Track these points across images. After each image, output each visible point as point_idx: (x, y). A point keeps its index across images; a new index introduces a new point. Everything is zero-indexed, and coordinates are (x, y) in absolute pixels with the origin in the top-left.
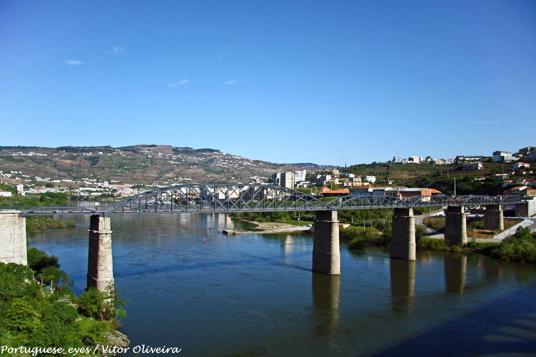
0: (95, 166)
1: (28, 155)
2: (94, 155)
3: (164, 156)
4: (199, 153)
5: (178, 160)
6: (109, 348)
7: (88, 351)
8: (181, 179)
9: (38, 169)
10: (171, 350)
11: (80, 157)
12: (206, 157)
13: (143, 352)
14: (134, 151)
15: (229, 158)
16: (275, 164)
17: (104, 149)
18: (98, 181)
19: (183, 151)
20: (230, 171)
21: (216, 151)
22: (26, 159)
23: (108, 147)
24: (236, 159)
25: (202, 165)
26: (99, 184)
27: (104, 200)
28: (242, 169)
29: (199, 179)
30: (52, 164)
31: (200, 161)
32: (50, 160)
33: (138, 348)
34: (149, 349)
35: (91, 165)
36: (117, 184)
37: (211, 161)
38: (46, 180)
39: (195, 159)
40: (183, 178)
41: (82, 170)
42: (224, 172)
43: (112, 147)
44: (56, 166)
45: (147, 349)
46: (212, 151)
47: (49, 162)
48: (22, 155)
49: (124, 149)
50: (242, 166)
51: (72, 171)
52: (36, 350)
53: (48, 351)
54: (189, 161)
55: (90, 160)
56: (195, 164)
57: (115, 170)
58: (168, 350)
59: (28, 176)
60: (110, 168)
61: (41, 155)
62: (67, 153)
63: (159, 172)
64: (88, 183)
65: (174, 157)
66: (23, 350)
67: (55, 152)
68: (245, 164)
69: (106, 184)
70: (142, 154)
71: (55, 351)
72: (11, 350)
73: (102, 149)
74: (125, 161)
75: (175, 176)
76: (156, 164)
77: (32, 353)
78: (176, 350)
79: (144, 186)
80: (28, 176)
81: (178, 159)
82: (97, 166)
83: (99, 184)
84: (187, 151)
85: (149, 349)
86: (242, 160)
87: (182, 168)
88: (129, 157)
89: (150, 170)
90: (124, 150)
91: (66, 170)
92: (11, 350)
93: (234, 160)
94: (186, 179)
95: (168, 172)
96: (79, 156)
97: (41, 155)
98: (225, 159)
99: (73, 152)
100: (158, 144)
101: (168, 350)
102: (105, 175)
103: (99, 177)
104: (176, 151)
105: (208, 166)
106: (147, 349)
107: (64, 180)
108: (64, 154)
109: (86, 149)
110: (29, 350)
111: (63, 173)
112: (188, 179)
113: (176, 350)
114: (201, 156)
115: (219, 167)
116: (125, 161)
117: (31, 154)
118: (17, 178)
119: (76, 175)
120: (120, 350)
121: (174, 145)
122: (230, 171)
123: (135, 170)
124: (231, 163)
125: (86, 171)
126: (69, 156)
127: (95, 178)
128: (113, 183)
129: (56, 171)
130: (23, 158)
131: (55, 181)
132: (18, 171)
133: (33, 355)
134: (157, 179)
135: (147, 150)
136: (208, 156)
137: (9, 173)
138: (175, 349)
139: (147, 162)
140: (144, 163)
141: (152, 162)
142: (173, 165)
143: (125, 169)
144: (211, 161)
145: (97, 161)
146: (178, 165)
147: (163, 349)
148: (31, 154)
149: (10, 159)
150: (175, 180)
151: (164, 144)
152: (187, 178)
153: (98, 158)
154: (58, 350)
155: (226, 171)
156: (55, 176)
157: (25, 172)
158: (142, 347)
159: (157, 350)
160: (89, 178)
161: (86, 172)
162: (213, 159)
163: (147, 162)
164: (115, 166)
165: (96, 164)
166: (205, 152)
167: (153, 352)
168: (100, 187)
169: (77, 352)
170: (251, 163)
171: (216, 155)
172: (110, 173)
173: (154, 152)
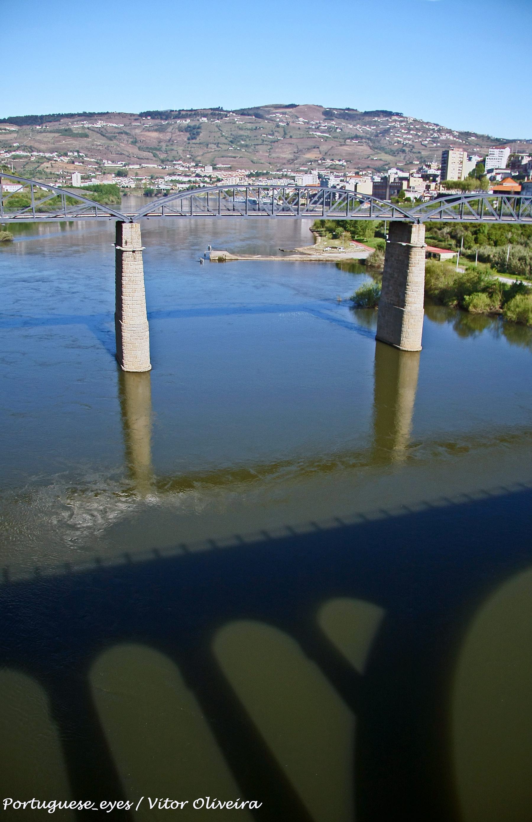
0: (194, 141)
1: (95, 126)
2: (192, 124)
3: (308, 123)
4: (367, 119)
5: (329, 130)
6: (158, 801)
7: (129, 806)
8: (329, 162)
9: (107, 148)
10: (248, 804)
11: (171, 127)
12: (377, 126)
13: (207, 808)
14: (257, 116)
15: (420, 127)
16: (497, 140)
17: (210, 112)
18: (197, 166)
19: (340, 115)
20: (414, 150)
21: (397, 114)
22: (91, 132)
23: (217, 109)
24: (429, 130)
25: (368, 139)
26: (198, 171)
27: (179, 474)
28: (436, 147)
29: (357, 163)
30: (131, 140)
31: (367, 132)
32: (127, 134)
33: (200, 801)
34: (216, 803)
35: (189, 139)
36: (226, 169)
37: (386, 132)
38: (119, 165)
39: (359, 129)
40: (332, 160)
41: (174, 147)
42: (404, 151)
43: (224, 109)
44: (136, 142)
45: (213, 803)
46: (389, 114)
47: (124, 136)
48: (86, 126)
49: (243, 113)
50: (438, 142)
51: (159, 150)
52: (54, 805)
53: (70, 806)
54: (348, 131)
55: (186, 131)
56: (356, 137)
57: (224, 147)
58: (243, 805)
59: (92, 160)
60: (217, 144)
61: (115, 125)
62: (153, 121)
63: (296, 150)
64: (181, 169)
65: (324, 125)
66: (35, 804)
67: (136, 120)
68: (443, 138)
69: (209, 170)
70: (271, 120)
71: (82, 806)
72: (17, 805)
73: (206, 112)
74: (241, 133)
75: (321, 156)
76: (291, 137)
77: (48, 809)
78: (255, 805)
79: (267, 173)
80: (92, 160)
81: (329, 128)
82: (197, 141)
83: (198, 171)
84: (348, 115)
85: (216, 803)
86: (439, 131)
87: (333, 144)
88: (249, 126)
89: (281, 148)
90: (243, 114)
91: (151, 148)
92: (17, 805)
93: (425, 131)
94: (337, 162)
95: (309, 150)
96: (171, 124)
97: (115, 125)
98: (409, 130)
99: (162, 119)
100: (301, 104)
101: (243, 805)
102: (209, 155)
103: (199, 158)
104: (329, 114)
105: (379, 142)
106: (213, 803)
107: (146, 165)
108: (149, 122)
109: (184, 113)
110: (44, 804)
111: (145, 154)
112: (341, 163)
113: (255, 805)
114: (370, 124)
115: (399, 142)
116: (241, 133)
117: (99, 124)
118: (76, 163)
119: (165, 155)
120: (175, 805)
121: (327, 105)
122: (414, 150)
123: (257, 147)
124: (419, 137)
125: (180, 149)
126: (157, 125)
127: (193, 161)
128: (220, 169)
129: (136, 151)
130: (87, 131)
131: (131, 167)
132: (78, 152)
133: (49, 811)
134: (291, 161)
135: (283, 113)
136: (382, 124)
137: (66, 155)
138: (253, 804)
139: (276, 134)
140: (273, 135)
141: (285, 134)
142: (319, 139)
143: (242, 146)
144: (386, 132)
145: (198, 133)
146: (326, 139)
147: (236, 804)
148: (99, 124)
149: (68, 133)
150: (319, 165)
151: (310, 103)
152: (339, 161)
153: (199, 128)
154: (85, 805)
155: (407, 149)
156: (133, 159)
157: (89, 154)
158: (206, 800)
159: (228, 805)
160: (184, 161)
161: (180, 152)
162: (389, 129)
163: (276, 134)
164: (226, 141)
165: (195, 138)
166: (378, 116)
167: (221, 808)
168: (198, 176)
169: (112, 808)
170: (454, 137)
171: (395, 121)
172: (216, 153)
173: (292, 116)
